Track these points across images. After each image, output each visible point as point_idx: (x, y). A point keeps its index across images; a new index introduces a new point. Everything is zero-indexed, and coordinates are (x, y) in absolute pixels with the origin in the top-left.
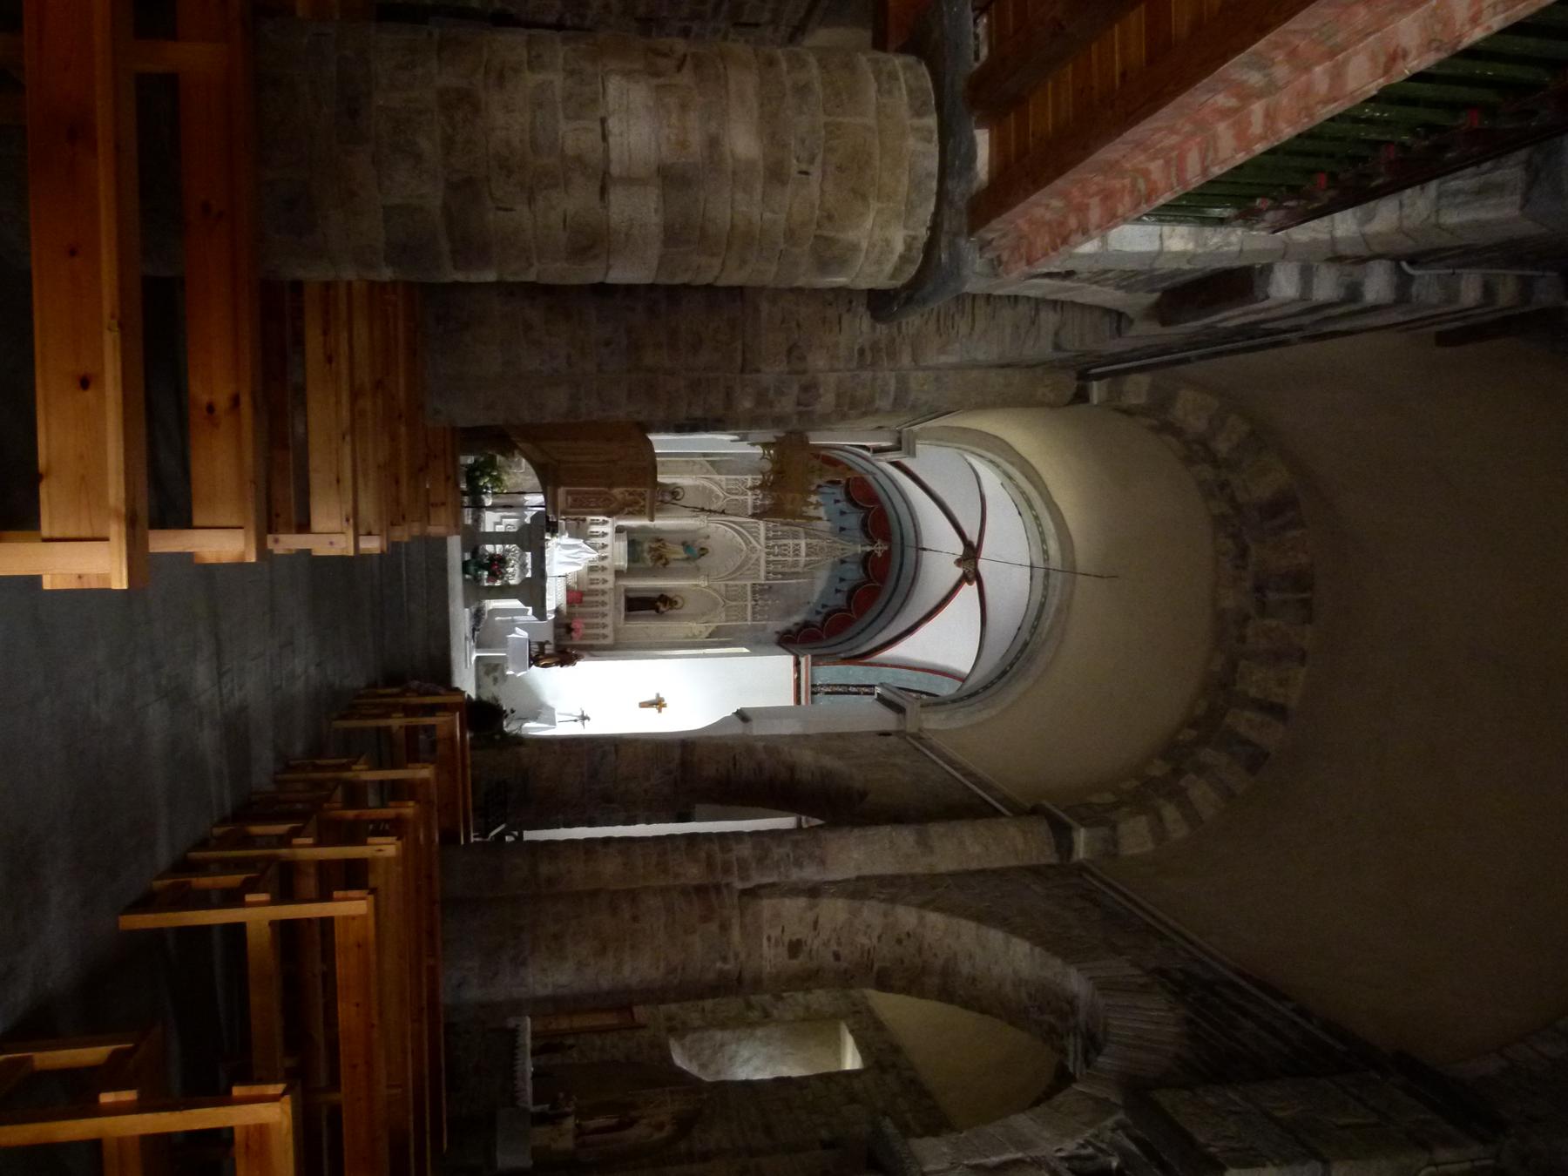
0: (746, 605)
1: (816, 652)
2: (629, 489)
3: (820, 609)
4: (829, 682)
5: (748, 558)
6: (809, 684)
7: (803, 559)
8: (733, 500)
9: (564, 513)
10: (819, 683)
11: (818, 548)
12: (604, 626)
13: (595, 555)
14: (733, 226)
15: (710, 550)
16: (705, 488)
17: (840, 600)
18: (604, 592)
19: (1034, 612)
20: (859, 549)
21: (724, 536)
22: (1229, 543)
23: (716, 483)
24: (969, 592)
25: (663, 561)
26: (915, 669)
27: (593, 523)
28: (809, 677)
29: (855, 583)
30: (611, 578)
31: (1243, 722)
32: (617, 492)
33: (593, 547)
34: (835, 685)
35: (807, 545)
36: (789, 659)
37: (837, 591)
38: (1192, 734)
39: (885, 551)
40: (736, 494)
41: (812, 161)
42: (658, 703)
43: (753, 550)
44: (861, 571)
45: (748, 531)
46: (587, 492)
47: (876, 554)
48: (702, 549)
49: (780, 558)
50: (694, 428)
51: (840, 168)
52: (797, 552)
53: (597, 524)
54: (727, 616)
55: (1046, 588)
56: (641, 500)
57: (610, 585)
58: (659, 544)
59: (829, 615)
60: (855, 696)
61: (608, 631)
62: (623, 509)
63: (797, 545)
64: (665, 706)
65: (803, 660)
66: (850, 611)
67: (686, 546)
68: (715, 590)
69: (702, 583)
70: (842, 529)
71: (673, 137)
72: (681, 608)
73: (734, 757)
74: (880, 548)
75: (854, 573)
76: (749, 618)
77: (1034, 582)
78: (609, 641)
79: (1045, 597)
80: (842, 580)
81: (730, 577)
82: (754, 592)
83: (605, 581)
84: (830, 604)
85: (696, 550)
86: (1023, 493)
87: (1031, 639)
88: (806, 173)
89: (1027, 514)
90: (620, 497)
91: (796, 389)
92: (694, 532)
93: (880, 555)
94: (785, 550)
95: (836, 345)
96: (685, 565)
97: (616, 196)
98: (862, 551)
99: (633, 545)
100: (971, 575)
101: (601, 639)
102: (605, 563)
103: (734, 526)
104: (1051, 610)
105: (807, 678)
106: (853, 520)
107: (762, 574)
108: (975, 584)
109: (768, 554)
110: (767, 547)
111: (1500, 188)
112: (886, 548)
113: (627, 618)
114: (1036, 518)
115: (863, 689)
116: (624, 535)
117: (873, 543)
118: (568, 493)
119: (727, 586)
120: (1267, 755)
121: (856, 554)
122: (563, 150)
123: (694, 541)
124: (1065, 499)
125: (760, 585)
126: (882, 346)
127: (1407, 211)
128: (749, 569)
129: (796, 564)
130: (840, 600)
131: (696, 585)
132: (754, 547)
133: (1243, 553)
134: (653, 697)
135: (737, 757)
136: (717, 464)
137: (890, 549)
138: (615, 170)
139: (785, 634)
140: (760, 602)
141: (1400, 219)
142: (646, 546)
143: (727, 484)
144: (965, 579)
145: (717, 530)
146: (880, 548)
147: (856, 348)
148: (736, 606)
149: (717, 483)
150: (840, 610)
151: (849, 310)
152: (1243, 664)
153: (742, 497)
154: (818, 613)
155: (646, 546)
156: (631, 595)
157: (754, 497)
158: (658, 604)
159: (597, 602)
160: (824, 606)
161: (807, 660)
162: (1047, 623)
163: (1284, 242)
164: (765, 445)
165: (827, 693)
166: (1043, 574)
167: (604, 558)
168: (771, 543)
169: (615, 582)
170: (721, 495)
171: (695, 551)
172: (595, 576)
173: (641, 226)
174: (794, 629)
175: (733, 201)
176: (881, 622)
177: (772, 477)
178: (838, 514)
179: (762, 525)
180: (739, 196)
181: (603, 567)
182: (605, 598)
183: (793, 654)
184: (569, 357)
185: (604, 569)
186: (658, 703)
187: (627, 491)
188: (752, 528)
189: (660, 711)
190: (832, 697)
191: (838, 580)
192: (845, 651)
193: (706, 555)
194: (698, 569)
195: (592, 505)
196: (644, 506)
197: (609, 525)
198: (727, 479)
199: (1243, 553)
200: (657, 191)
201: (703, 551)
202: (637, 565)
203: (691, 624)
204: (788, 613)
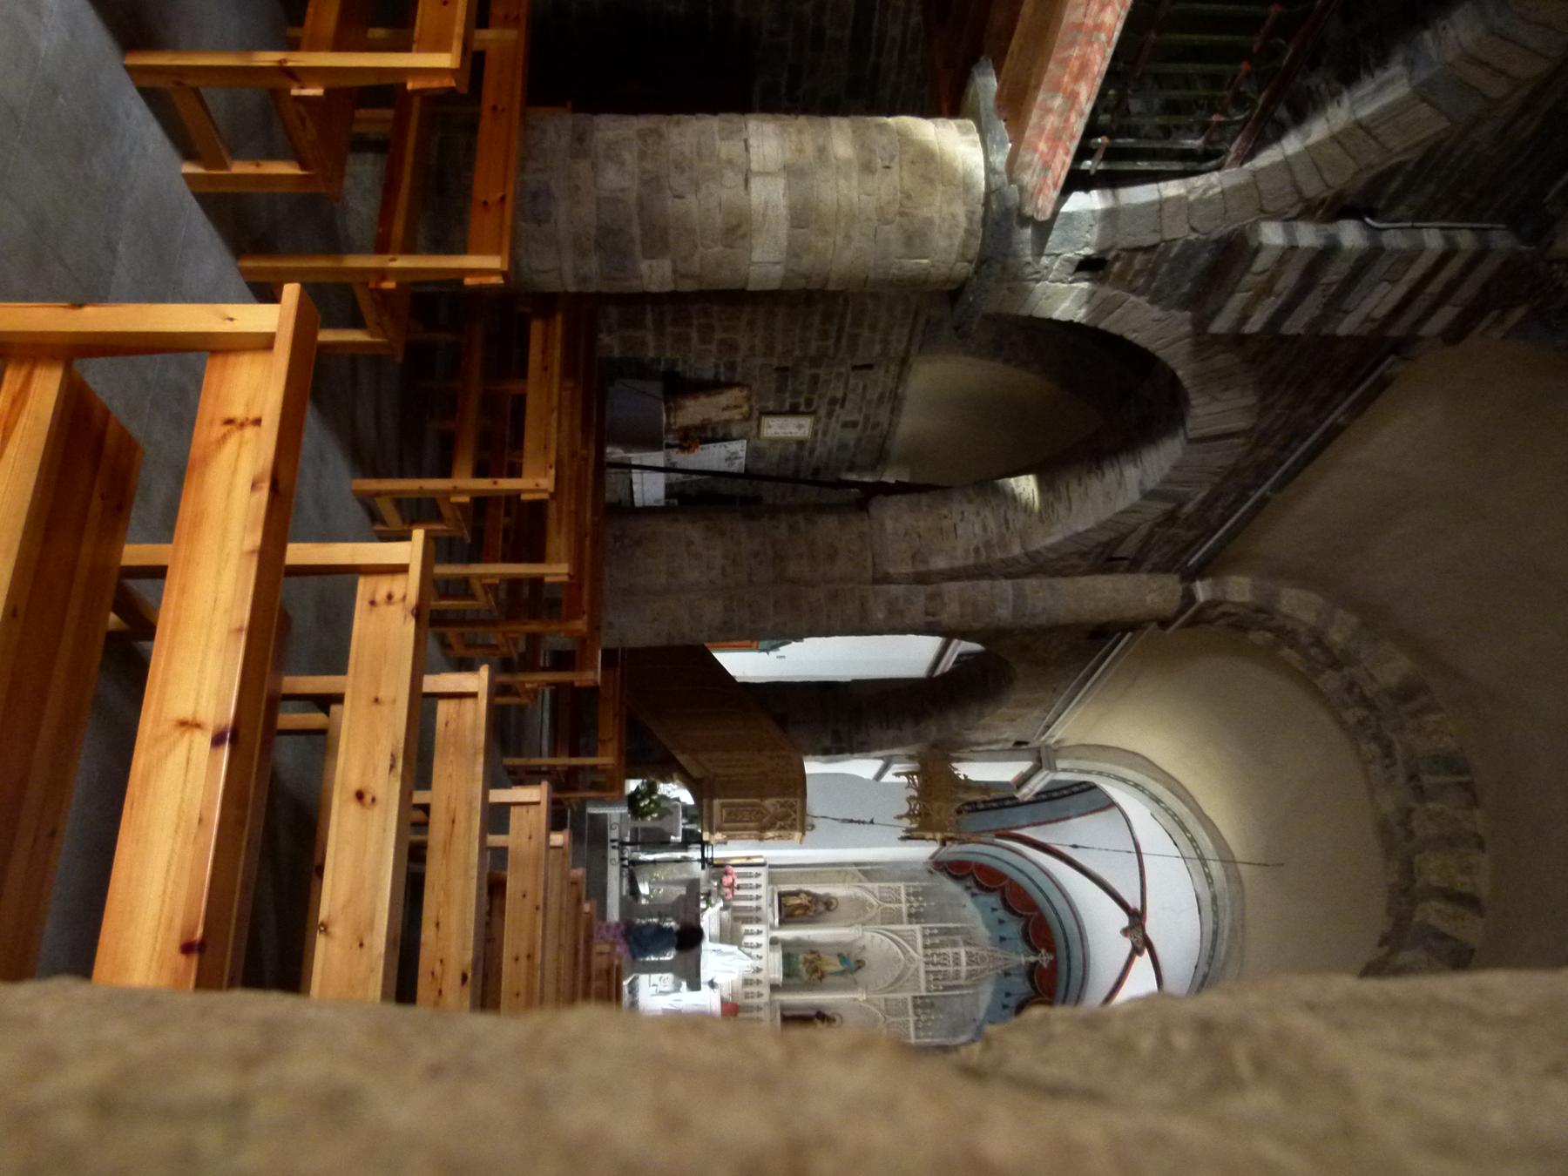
0: (908, 1021)
2: (780, 800)
5: (906, 968)
8: (886, 908)
9: (720, 829)
14: (839, 205)
15: (867, 962)
16: (857, 899)
18: (759, 1009)
19: (1208, 945)
20: (1023, 959)
21: (880, 946)
22: (1374, 747)
23: (870, 892)
24: (1143, 962)
27: (748, 933)
29: (1022, 998)
30: (766, 991)
31: (1433, 913)
32: (770, 803)
35: (967, 952)
37: (1005, 1007)
38: (1386, 949)
39: (1051, 962)
40: (890, 902)
41: (892, 158)
43: (911, 960)
45: (906, 941)
46: (740, 805)
47: (1041, 965)
48: (859, 961)
50: (836, 774)
51: (913, 163)
52: (957, 962)
55: (1215, 913)
56: (792, 813)
57: (765, 998)
62: (775, 824)
63: (957, 954)
67: (842, 958)
68: (875, 1005)
69: (861, 996)
70: (1002, 939)
71: (793, 147)
74: (1044, 958)
77: (1203, 913)
79: (1216, 923)
80: (1008, 995)
81: (890, 989)
82: (915, 1006)
83: (760, 995)
85: (852, 962)
86: (1174, 815)
87: (1209, 969)
88: (888, 167)
89: (1183, 840)
90: (772, 810)
91: (922, 598)
92: (850, 944)
93: (1045, 965)
94: (945, 959)
95: (954, 548)
97: (755, 184)
98: (1026, 962)
99: (788, 959)
100: (1142, 944)
102: (760, 976)
103: (891, 935)
104: (1225, 933)
106: (1013, 928)
107: (923, 985)
108: (1146, 952)
110: (926, 956)
111: (1391, 81)
112: (1051, 958)
114: (1192, 840)
116: (779, 947)
117: (1036, 951)
118: (723, 806)
119: (886, 1000)
120: (1472, 951)
121: (1020, 965)
122: (718, 156)
123: (849, 954)
124: (1216, 806)
125: (921, 997)
126: (995, 541)
127: (1333, 122)
128: (908, 980)
129: (957, 975)
131: (855, 999)
133: (1388, 750)
136: (868, 871)
137: (1056, 958)
138: (754, 167)
141: (1329, 128)
142: (801, 958)
143: (880, 892)
144: (1135, 951)
145: (874, 940)
146: (1045, 958)
147: (972, 548)
151: (962, 520)
152: (1417, 859)
153: (897, 906)
155: (801, 958)
157: (908, 905)
162: (1222, 949)
163: (1251, 171)
164: (907, 774)
166: (1210, 906)
167: (758, 970)
168: (929, 952)
170: (875, 903)
171: (852, 964)
172: (749, 989)
173: (773, 207)
175: (838, 186)
177: (918, 807)
178: (997, 923)
179: (917, 927)
180: (842, 182)
182: (761, 1014)
184: (723, 568)
185: (759, 982)
187: (778, 802)
188: (908, 936)
191: (1003, 995)
193: (863, 968)
195: (745, 819)
196: (795, 820)
198: (880, 887)
199: (1388, 750)
200: (783, 181)
201: (860, 964)
202: (792, 981)
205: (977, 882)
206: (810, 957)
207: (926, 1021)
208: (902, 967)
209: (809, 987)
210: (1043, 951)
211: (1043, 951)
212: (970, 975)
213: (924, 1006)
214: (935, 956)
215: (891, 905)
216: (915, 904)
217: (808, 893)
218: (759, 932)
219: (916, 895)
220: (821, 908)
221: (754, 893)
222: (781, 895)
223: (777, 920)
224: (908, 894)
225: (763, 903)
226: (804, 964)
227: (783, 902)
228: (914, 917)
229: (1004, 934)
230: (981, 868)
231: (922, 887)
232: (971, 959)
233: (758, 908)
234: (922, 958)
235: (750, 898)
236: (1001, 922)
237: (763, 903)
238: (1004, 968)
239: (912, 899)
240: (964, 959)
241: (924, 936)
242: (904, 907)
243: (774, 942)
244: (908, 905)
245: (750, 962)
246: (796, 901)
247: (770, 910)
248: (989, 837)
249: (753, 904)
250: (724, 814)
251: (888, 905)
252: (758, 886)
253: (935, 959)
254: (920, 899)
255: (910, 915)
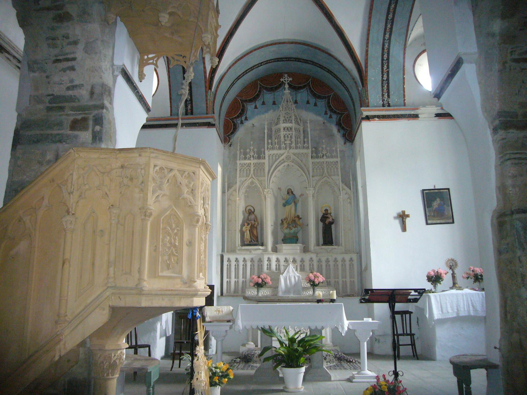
1: (357, 104)
2: (151, 189)
3: (328, 116)
4: (381, 95)
6: (382, 108)
7: (293, 125)
9: (191, 281)
10: (381, 102)
11: (287, 116)
12: (343, 260)
13: (291, 267)
17: (322, 103)
18: (320, 261)
20: (287, 91)
25: (297, 219)
26: (369, 26)
28: (378, 108)
30: (307, 257)
33: (286, 267)
34: (383, 90)
36: (365, 125)
37: (315, 105)
40: (250, 170)
42: (402, 217)
43: (288, 158)
44: (302, 90)
45: (276, 161)
48: (288, 193)
49: (293, 140)
53: (270, 265)
54: (334, 175)
57: (314, 256)
58: (284, 222)
59: (331, 110)
60: (390, 76)
61: (347, 257)
63: (284, 129)
64: (404, 212)
65: (365, 114)
66: (329, 97)
70: (274, 103)
72: (330, 207)
73: (517, 61)
74: (286, 79)
75: (303, 95)
76: (335, 160)
78: (355, 257)
80: (308, 102)
81: (307, 172)
82: (317, 157)
83: (311, 259)
84: (324, 109)
92: (276, 198)
96: (299, 205)
99: (287, 240)
101: (353, 263)
102: (298, 259)
105: (379, 110)
106: (268, 97)
107: (305, 151)
109: (290, 148)
110: (286, 148)
112: (286, 75)
113: (338, 244)
115: (385, 69)
116: (278, 246)
117: (283, 83)
118: (154, 274)
125: (312, 153)
130: (322, 103)
132: (286, 158)
134: (397, 224)
135: (516, 57)
139: (346, 138)
140: (324, 153)
146: (286, 79)
148: (327, 169)
149: (242, 183)
150: (329, 103)
153: (252, 166)
154: (331, 117)
156: (321, 241)
157: (252, 158)
158: (327, 222)
159: (326, 266)
160: (326, 113)
161: (365, 111)
165: (389, 96)
167: (294, 261)
169: (312, 252)
170: (250, 180)
172: (307, 267)
174: (342, 132)
176: (335, 67)
181: (301, 262)
182: (324, 259)
183: (361, 122)
185: (302, 261)
186: (402, 217)
187: (154, 192)
188: (272, 159)
189: (408, 216)
190: (391, 93)
192: (357, 87)
194: (302, 195)
196: (182, 172)
197: (270, 256)
201: (290, 192)
203: (341, 200)
204: (331, 136)
205: (238, 117)
206: (285, 225)
207: (327, 151)
208: (293, 164)
209: (305, 226)
210: (282, 80)
211: (282, 80)
212: (297, 123)
213: (316, 153)
214: (286, 142)
215: (252, 170)
216: (252, 154)
217: (243, 225)
218: (269, 260)
219: (245, 154)
220: (252, 217)
221: (241, 263)
222: (243, 244)
223: (261, 247)
224: (245, 158)
225: (248, 257)
226: (291, 229)
227: (248, 243)
228: (260, 155)
229: (271, 103)
230: (229, 113)
231: (240, 149)
232: (285, 121)
233: (252, 260)
234: (287, 151)
235: (245, 266)
236: (263, 103)
237: (248, 257)
238: (292, 103)
239: (248, 156)
240: (288, 125)
241: (273, 148)
242: (253, 161)
243: (275, 250)
244: (252, 158)
245: (291, 267)
246: (247, 235)
247: (253, 252)
248: (210, 97)
249: (249, 264)
250: (166, 273)
251: (252, 172)
252: (237, 260)
253: (288, 142)
254: (248, 150)
255: (259, 158)
